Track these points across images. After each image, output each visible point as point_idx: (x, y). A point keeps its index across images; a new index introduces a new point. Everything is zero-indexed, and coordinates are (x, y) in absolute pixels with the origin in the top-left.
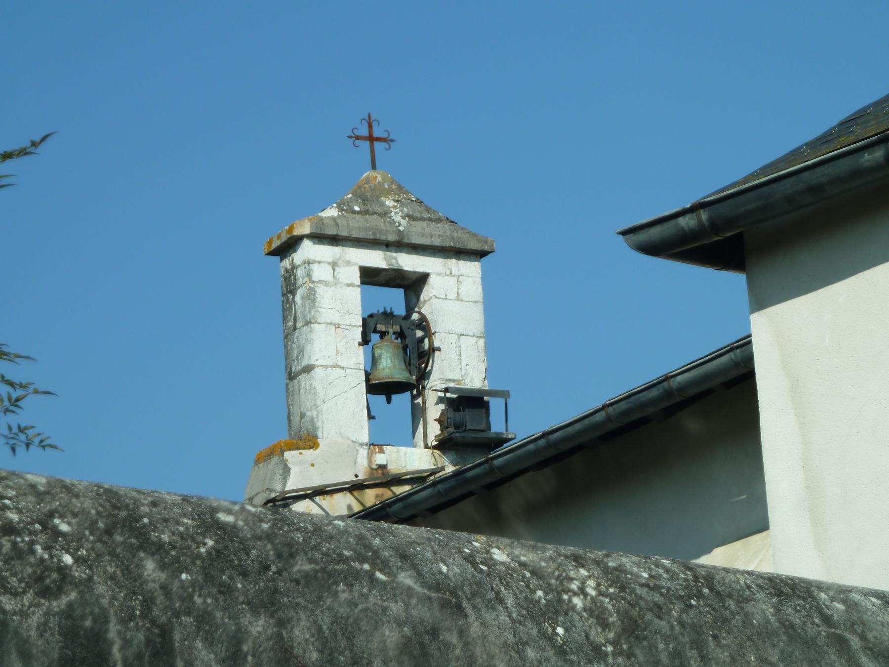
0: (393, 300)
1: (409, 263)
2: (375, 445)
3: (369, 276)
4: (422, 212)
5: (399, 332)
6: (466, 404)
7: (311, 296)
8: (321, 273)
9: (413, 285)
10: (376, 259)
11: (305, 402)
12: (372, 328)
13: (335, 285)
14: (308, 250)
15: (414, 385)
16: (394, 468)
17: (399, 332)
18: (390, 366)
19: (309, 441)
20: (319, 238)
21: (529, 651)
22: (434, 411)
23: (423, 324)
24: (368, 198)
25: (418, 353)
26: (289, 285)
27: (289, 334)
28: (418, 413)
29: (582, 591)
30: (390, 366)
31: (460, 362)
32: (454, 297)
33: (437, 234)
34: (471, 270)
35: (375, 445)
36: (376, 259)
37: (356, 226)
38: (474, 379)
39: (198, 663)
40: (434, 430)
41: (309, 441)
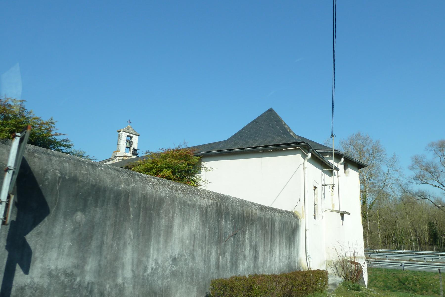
0: (129, 138)
1: (132, 135)
2: (126, 153)
3: (127, 136)
4: (133, 130)
5: (130, 142)
6: (135, 150)
7: (121, 137)
8: (123, 135)
9: (131, 137)
10: (128, 134)
11: (119, 147)
12: (127, 141)
13: (124, 136)
14: (122, 132)
15: (130, 147)
16: (127, 155)
17: (130, 142)
18: (128, 145)
19: (119, 151)
20: (123, 131)
21: (164, 220)
22: (132, 150)
23: (132, 141)
24: (128, 128)
25: (131, 145)
26: (119, 135)
27: (118, 140)
28: (130, 150)
29: (169, 160)
30: (128, 145)
31: (135, 146)
32: (135, 139)
33: (135, 133)
34: (137, 137)
35: (126, 153)
36: (128, 134)
37: (127, 131)
38: (136, 148)
39: (434, 192)
40: (131, 152)
41: (119, 151)
